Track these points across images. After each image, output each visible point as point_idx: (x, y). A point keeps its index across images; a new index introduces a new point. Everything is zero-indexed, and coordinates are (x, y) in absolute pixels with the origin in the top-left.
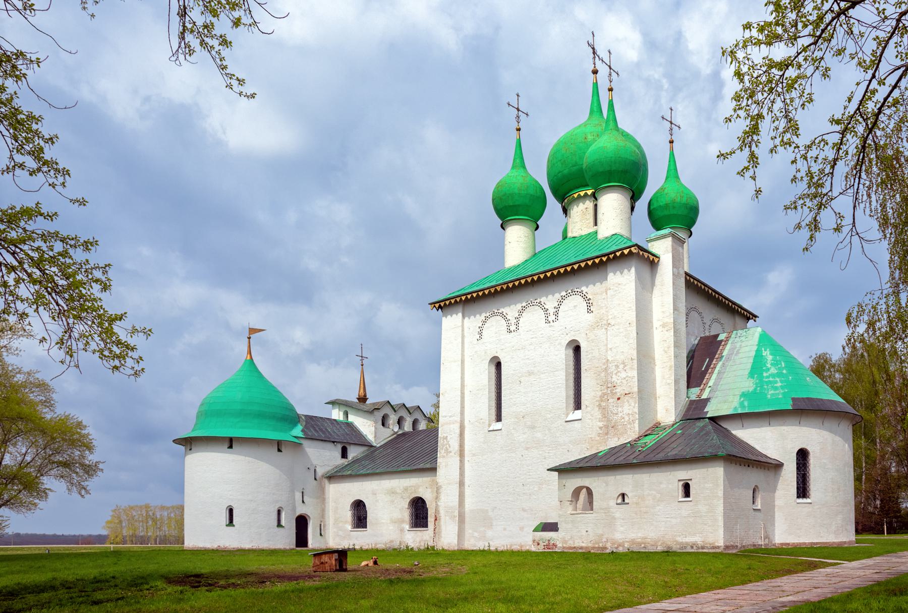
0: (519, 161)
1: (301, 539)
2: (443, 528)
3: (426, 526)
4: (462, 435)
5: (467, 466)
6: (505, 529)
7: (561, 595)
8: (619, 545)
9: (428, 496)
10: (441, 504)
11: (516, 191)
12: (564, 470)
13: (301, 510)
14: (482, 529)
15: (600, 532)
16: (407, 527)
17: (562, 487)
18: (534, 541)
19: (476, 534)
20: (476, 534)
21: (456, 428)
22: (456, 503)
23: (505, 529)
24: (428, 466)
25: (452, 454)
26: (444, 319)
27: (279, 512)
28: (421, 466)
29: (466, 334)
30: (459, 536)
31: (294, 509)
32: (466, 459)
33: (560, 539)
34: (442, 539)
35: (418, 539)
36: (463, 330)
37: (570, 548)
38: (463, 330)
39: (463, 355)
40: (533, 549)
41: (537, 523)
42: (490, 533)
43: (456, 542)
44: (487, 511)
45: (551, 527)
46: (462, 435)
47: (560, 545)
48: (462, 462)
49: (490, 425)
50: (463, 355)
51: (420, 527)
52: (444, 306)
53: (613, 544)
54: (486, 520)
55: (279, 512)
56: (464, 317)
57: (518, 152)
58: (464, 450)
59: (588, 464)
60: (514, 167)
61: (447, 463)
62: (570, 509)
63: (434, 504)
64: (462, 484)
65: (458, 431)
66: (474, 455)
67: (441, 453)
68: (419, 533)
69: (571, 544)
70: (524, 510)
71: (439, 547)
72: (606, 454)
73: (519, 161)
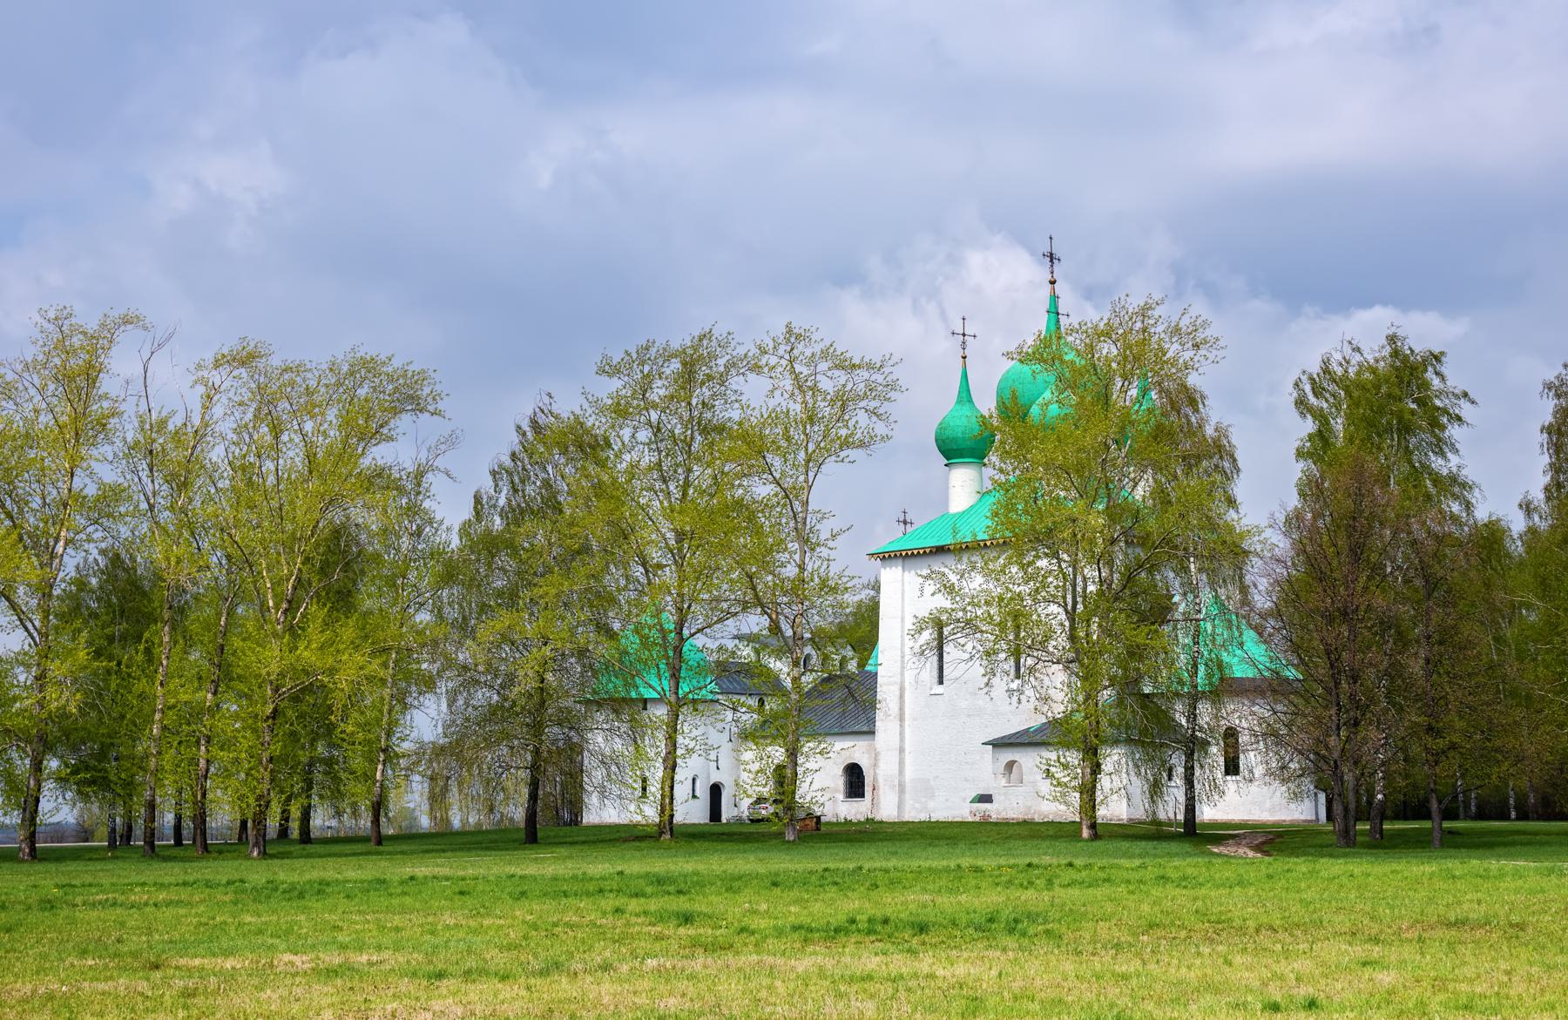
0: (965, 395)
1: (715, 812)
2: (882, 798)
3: (863, 796)
4: (902, 697)
5: (907, 730)
6: (947, 800)
7: (645, 702)
8: (1045, 817)
9: (865, 763)
10: (881, 772)
11: (960, 435)
12: (999, 744)
13: (715, 777)
14: (923, 800)
15: (1029, 804)
16: (841, 796)
17: (995, 760)
18: (971, 812)
19: (917, 805)
20: (917, 805)
21: (895, 689)
22: (897, 772)
23: (947, 800)
24: (865, 729)
25: (892, 718)
26: (882, 570)
27: (694, 780)
28: (856, 728)
29: (906, 588)
30: (899, 807)
31: (708, 777)
32: (907, 723)
33: (996, 811)
34: (881, 811)
35: (853, 811)
36: (903, 585)
37: (1004, 819)
38: (903, 585)
39: (903, 611)
40: (970, 819)
41: (974, 794)
42: (931, 804)
43: (896, 813)
44: (929, 780)
45: (986, 798)
46: (902, 697)
47: (994, 816)
48: (902, 709)
49: (931, 689)
50: (903, 611)
51: (856, 797)
52: (887, 557)
53: (1040, 815)
54: (927, 789)
55: (694, 780)
56: (904, 570)
57: (964, 383)
58: (904, 763)
59: (1018, 741)
60: (960, 401)
61: (885, 725)
62: (1003, 782)
63: (872, 771)
64: (902, 750)
65: (898, 693)
66: (915, 719)
67: (879, 715)
68: (855, 804)
69: (1004, 815)
70: (966, 780)
71: (878, 818)
72: (1036, 731)
73: (965, 395)
